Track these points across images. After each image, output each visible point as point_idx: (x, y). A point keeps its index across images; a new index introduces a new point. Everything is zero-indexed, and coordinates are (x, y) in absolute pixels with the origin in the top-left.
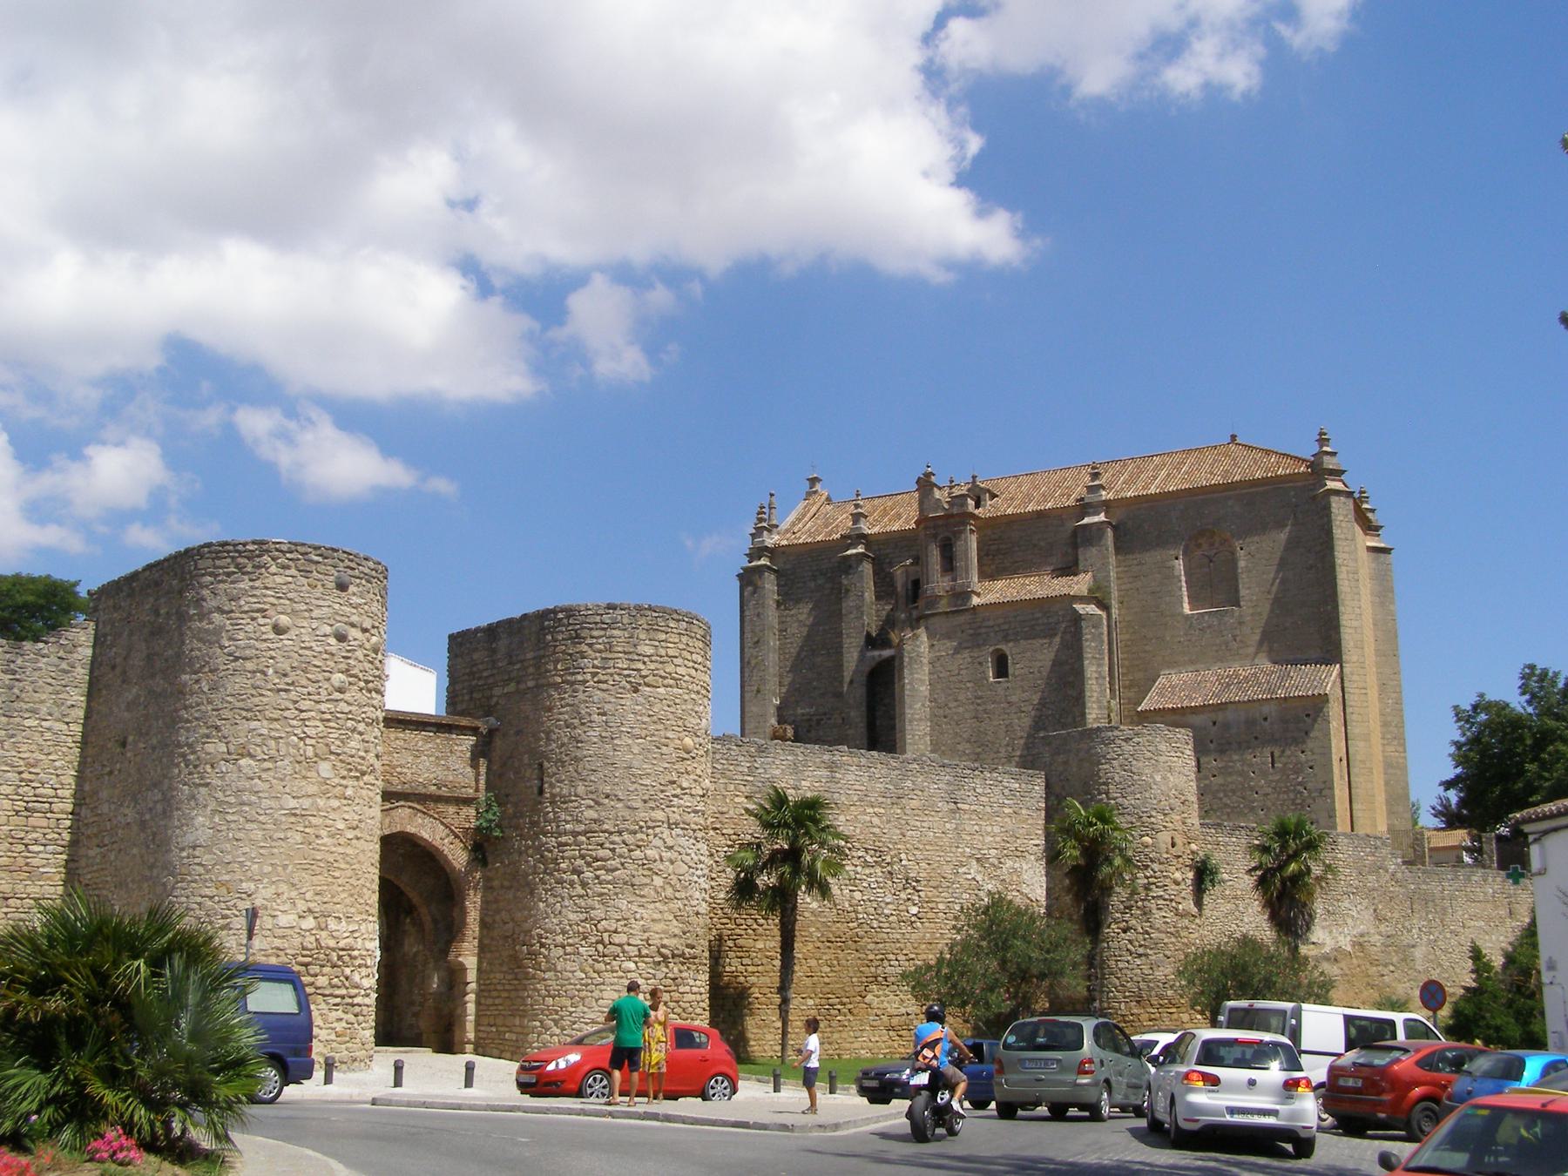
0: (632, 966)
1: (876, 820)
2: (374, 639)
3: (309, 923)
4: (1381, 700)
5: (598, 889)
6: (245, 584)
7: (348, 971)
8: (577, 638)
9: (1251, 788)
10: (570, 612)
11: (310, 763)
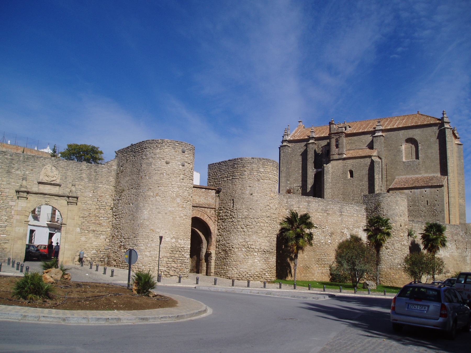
0: (256, 254)
1: (320, 217)
2: (191, 166)
3: (174, 240)
4: (458, 187)
5: (248, 233)
6: (158, 151)
7: (183, 253)
8: (244, 167)
9: (421, 210)
10: (241, 159)
11: (174, 199)
